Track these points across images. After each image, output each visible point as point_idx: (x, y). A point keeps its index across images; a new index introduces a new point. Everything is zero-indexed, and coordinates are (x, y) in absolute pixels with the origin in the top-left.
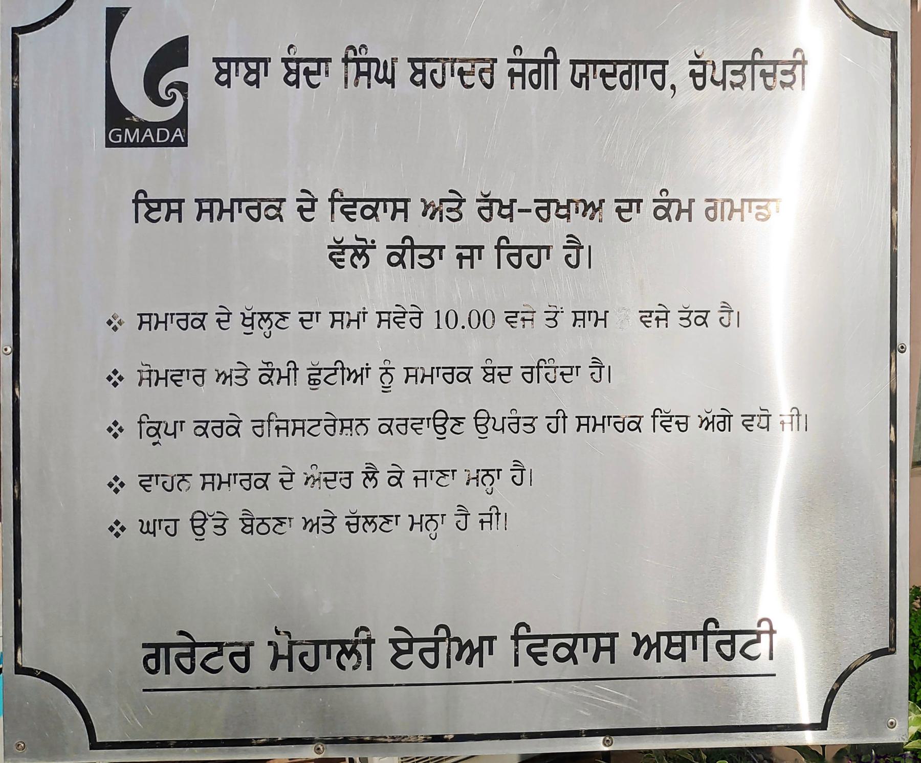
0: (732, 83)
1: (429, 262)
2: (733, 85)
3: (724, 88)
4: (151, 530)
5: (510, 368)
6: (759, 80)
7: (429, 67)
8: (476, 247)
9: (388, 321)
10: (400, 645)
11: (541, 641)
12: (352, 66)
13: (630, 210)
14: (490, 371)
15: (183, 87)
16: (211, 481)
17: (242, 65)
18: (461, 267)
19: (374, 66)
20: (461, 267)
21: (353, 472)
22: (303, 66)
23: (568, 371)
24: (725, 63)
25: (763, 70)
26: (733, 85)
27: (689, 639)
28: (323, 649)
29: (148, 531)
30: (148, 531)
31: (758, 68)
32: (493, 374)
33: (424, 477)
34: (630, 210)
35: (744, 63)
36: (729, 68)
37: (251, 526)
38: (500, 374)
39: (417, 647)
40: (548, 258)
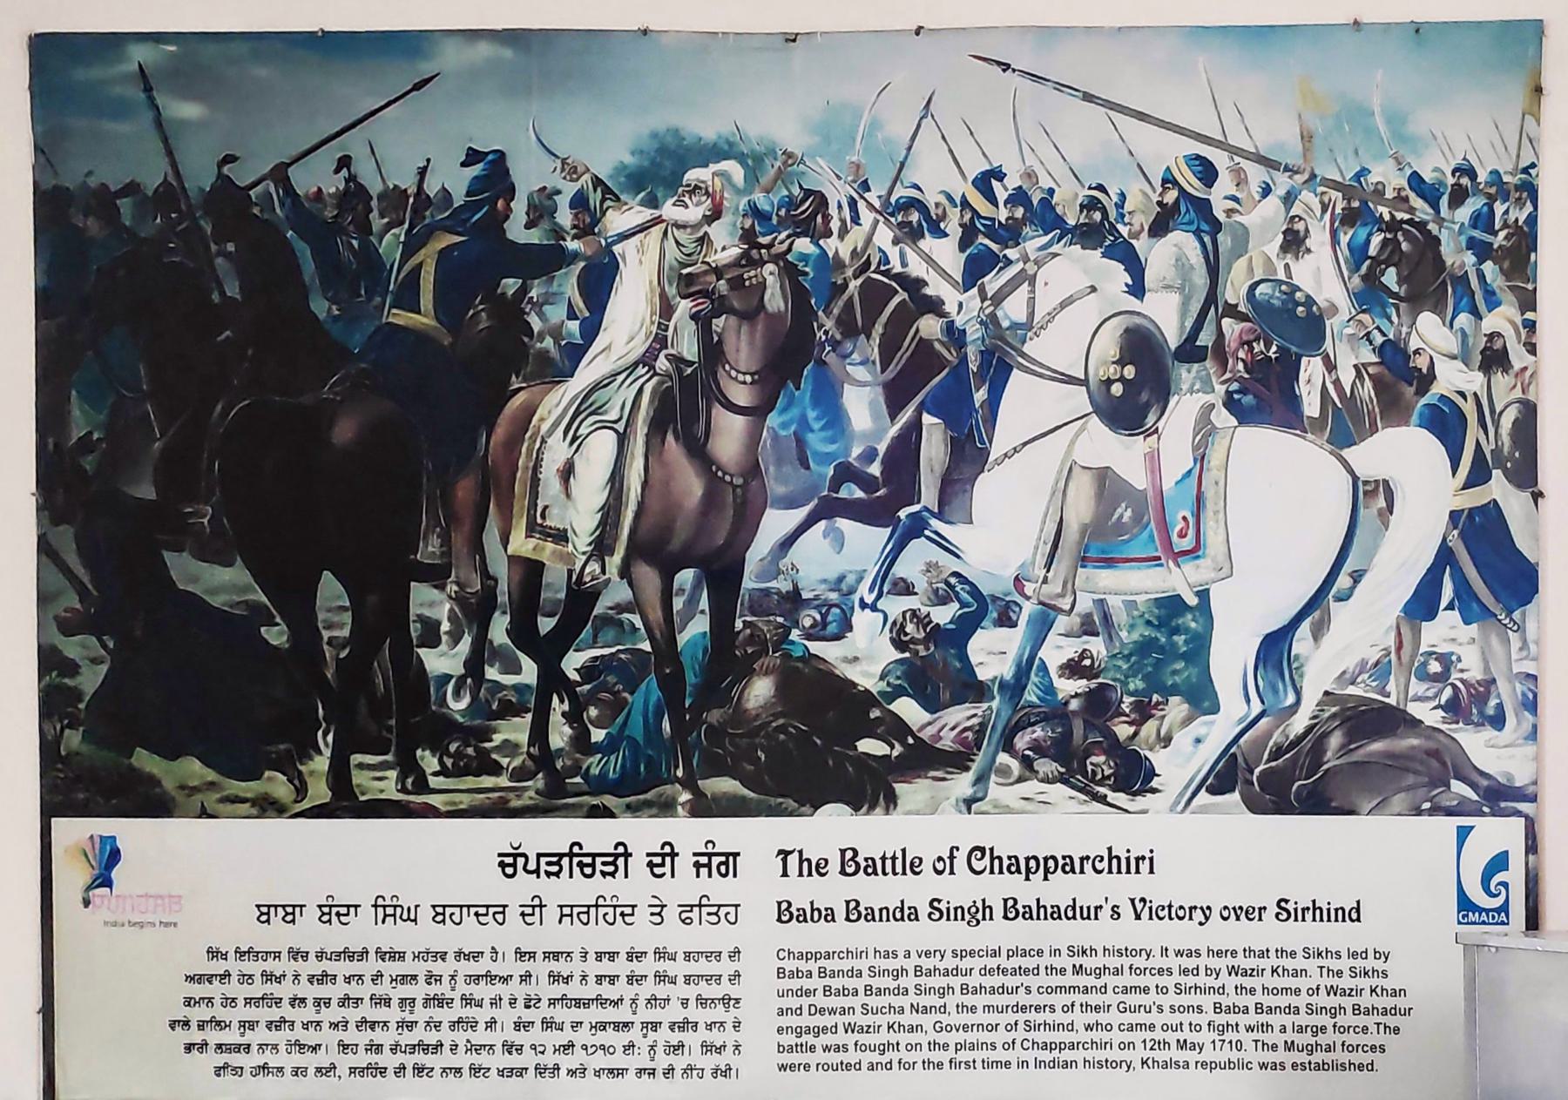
0: (546, 872)
1: (1117, 392)
2: (548, 874)
3: (538, 877)
4: (412, 917)
5: (633, 907)
6: (576, 870)
7: (448, 911)
8: (731, 854)
9: (571, 915)
10: (323, 909)
11: (689, 909)
12: (380, 910)
13: (347, 915)
14: (326, 910)
15: (1505, 885)
16: (392, 912)
17: (280, 909)
18: (698, 876)
19: (399, 910)
20: (698, 876)
21: (305, 906)
22: (334, 910)
23: (343, 910)
24: (539, 856)
25: (580, 862)
26: (548, 874)
27: (272, 909)
28: (465, 909)
29: (409, 919)
30: (409, 919)
31: (576, 860)
32: (330, 914)
33: (458, 909)
34: (347, 915)
35: (561, 856)
36: (543, 860)
37: (444, 914)
38: (338, 914)
39: (492, 910)
40: (301, 915)
